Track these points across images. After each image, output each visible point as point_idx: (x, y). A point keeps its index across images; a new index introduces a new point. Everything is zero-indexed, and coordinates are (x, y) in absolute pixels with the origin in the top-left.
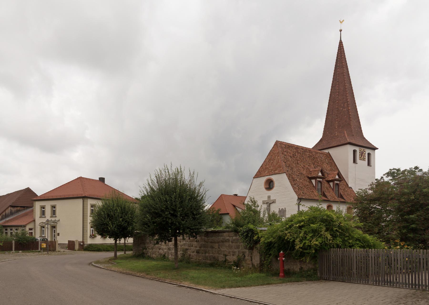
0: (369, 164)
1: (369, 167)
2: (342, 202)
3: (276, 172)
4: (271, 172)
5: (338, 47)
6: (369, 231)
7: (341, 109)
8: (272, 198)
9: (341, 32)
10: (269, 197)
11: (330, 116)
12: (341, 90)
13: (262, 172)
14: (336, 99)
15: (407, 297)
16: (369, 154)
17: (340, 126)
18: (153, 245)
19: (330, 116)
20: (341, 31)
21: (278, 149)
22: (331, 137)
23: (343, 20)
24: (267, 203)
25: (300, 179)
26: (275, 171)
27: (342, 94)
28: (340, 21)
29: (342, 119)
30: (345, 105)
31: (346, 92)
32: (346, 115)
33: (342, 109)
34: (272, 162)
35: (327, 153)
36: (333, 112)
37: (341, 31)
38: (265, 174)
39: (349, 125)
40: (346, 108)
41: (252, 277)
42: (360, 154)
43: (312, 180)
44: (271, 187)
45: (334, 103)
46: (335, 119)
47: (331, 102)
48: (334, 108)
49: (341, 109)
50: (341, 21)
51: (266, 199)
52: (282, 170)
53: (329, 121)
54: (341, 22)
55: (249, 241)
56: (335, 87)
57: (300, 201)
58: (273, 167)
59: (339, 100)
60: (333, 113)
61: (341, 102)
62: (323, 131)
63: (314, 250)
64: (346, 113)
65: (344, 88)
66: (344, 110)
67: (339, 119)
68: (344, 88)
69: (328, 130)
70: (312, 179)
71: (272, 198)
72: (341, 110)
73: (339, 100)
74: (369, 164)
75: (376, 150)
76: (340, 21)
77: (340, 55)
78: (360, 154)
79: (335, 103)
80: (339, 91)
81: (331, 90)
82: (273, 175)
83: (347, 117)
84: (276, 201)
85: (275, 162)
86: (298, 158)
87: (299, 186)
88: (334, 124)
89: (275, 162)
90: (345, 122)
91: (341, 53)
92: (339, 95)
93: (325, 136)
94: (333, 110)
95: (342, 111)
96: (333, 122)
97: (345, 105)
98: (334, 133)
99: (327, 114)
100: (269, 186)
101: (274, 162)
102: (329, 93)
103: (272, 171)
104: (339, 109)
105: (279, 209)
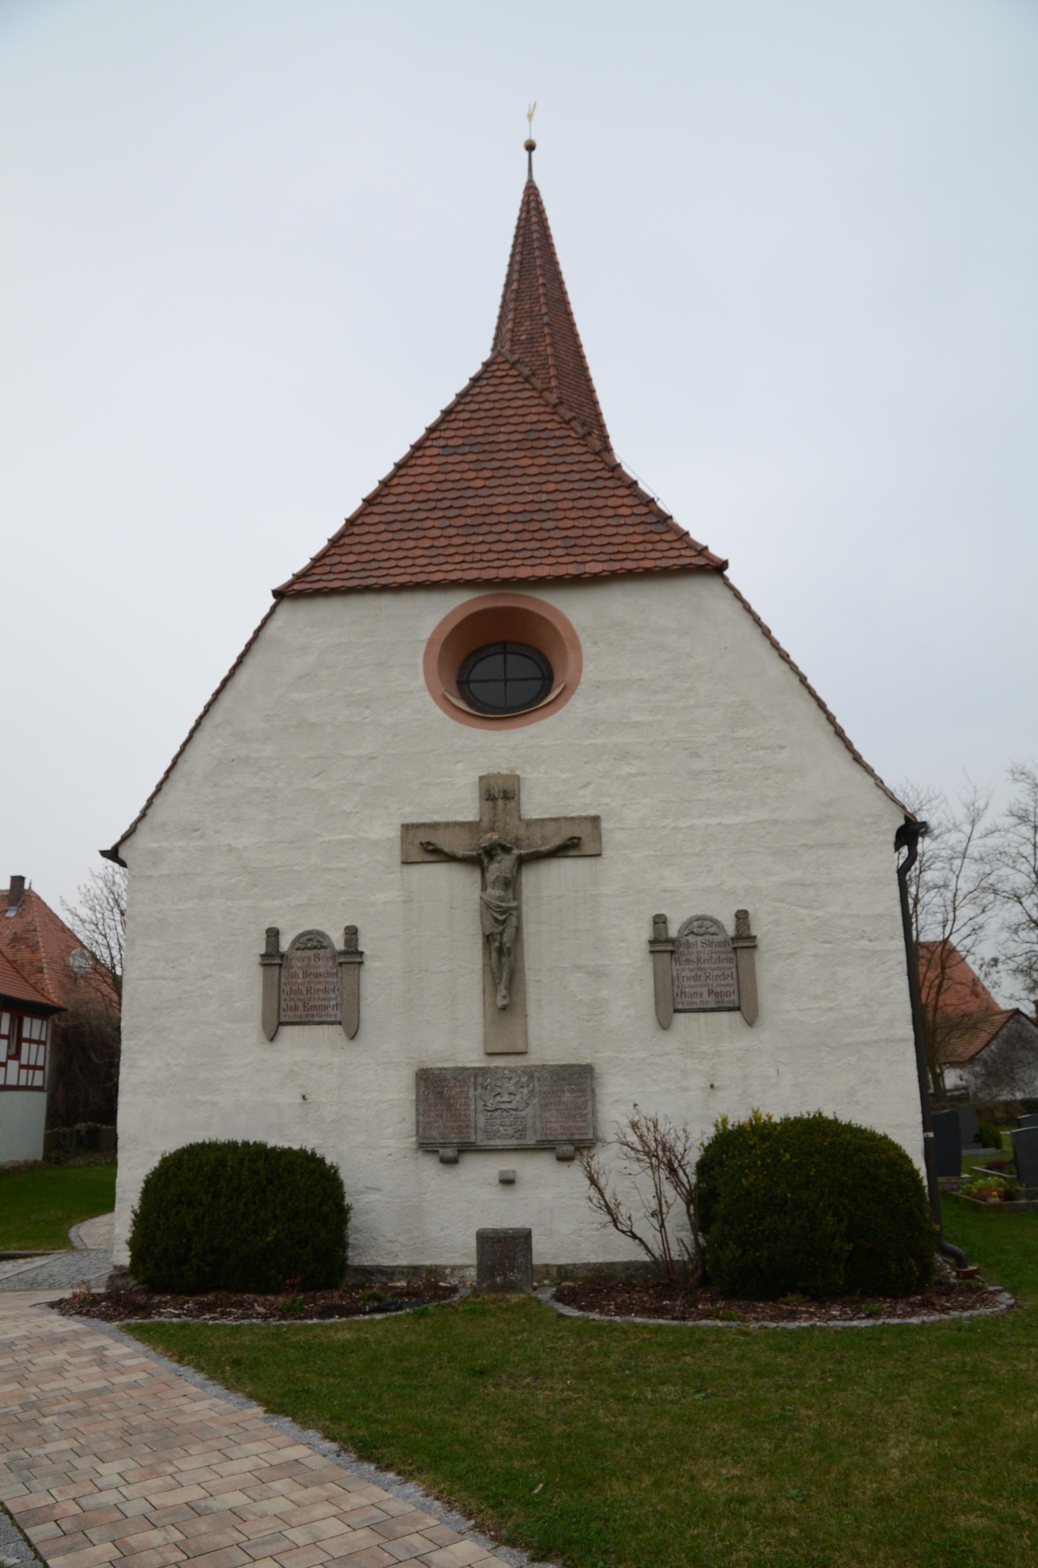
9: (534, 153)
20: (530, 147)
37: (530, 147)
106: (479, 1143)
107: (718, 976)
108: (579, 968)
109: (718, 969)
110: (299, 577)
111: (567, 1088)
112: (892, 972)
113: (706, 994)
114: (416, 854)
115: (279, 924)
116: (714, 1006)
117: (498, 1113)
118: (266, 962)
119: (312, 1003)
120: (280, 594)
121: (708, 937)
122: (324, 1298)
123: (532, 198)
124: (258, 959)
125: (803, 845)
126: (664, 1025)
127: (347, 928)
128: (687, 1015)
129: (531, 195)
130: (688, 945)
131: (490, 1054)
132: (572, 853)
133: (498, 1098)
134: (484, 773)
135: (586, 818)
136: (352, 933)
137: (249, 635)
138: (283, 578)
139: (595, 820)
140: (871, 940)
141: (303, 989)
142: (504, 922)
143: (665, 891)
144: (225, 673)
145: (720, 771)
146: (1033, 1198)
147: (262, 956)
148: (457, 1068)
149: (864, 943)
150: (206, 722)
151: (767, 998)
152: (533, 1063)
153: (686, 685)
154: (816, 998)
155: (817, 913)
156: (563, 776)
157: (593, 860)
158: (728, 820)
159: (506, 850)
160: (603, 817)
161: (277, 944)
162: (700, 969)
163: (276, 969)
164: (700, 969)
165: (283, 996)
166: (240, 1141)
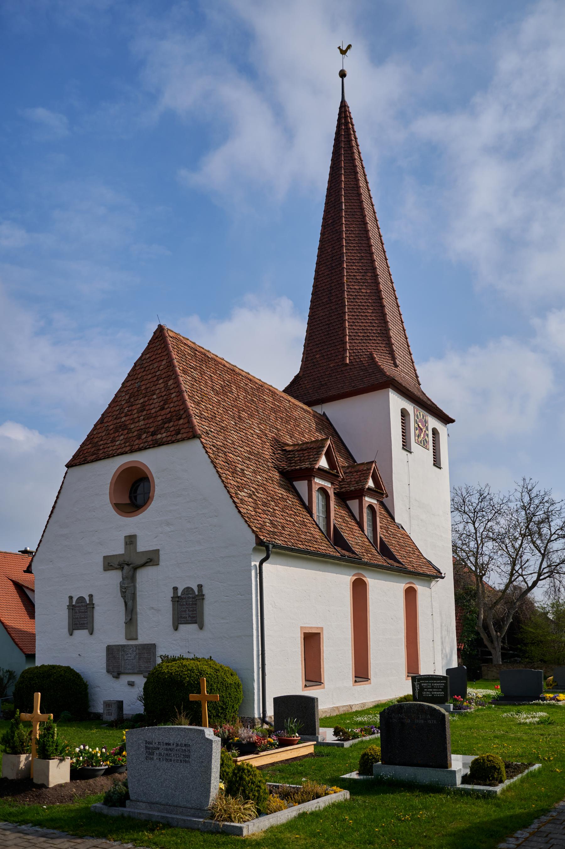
1: (162, 557)
2: (342, 559)
3: (159, 436)
4: (139, 438)
5: (339, 106)
8: (142, 546)
9: (345, 79)
10: (131, 540)
11: (323, 307)
13: (102, 442)
19: (323, 307)
20: (343, 74)
21: (165, 353)
22: (329, 369)
23: (349, 47)
24: (121, 567)
25: (254, 472)
26: (154, 434)
28: (339, 48)
34: (142, 401)
35: (320, 414)
37: (343, 74)
38: (115, 448)
43: (294, 483)
44: (140, 500)
48: (333, 285)
50: (344, 49)
51: (118, 549)
52: (185, 426)
54: (343, 52)
56: (335, 226)
57: (264, 556)
58: (146, 422)
60: (331, 298)
62: (303, 354)
69: (318, 349)
70: (296, 481)
71: (142, 546)
76: (341, 48)
79: (336, 270)
81: (322, 234)
82: (145, 449)
84: (161, 558)
85: (155, 401)
86: (241, 403)
87: (257, 497)
88: (337, 330)
89: (155, 401)
93: (309, 366)
96: (334, 324)
98: (340, 357)
100: (130, 498)
101: (149, 400)
103: (144, 436)
105: (175, 589)
106: (122, 671)
107: (192, 610)
110: (71, 460)
113: (188, 617)
117: (127, 661)
119: (81, 622)
120: (69, 466)
122: (426, 808)
123: (343, 110)
124: (171, 599)
126: (176, 629)
129: (344, 108)
132: (151, 564)
133: (127, 656)
136: (91, 596)
138: (68, 458)
139: (158, 551)
141: (79, 617)
142: (125, 592)
145: (197, 528)
147: (172, 597)
152: (141, 643)
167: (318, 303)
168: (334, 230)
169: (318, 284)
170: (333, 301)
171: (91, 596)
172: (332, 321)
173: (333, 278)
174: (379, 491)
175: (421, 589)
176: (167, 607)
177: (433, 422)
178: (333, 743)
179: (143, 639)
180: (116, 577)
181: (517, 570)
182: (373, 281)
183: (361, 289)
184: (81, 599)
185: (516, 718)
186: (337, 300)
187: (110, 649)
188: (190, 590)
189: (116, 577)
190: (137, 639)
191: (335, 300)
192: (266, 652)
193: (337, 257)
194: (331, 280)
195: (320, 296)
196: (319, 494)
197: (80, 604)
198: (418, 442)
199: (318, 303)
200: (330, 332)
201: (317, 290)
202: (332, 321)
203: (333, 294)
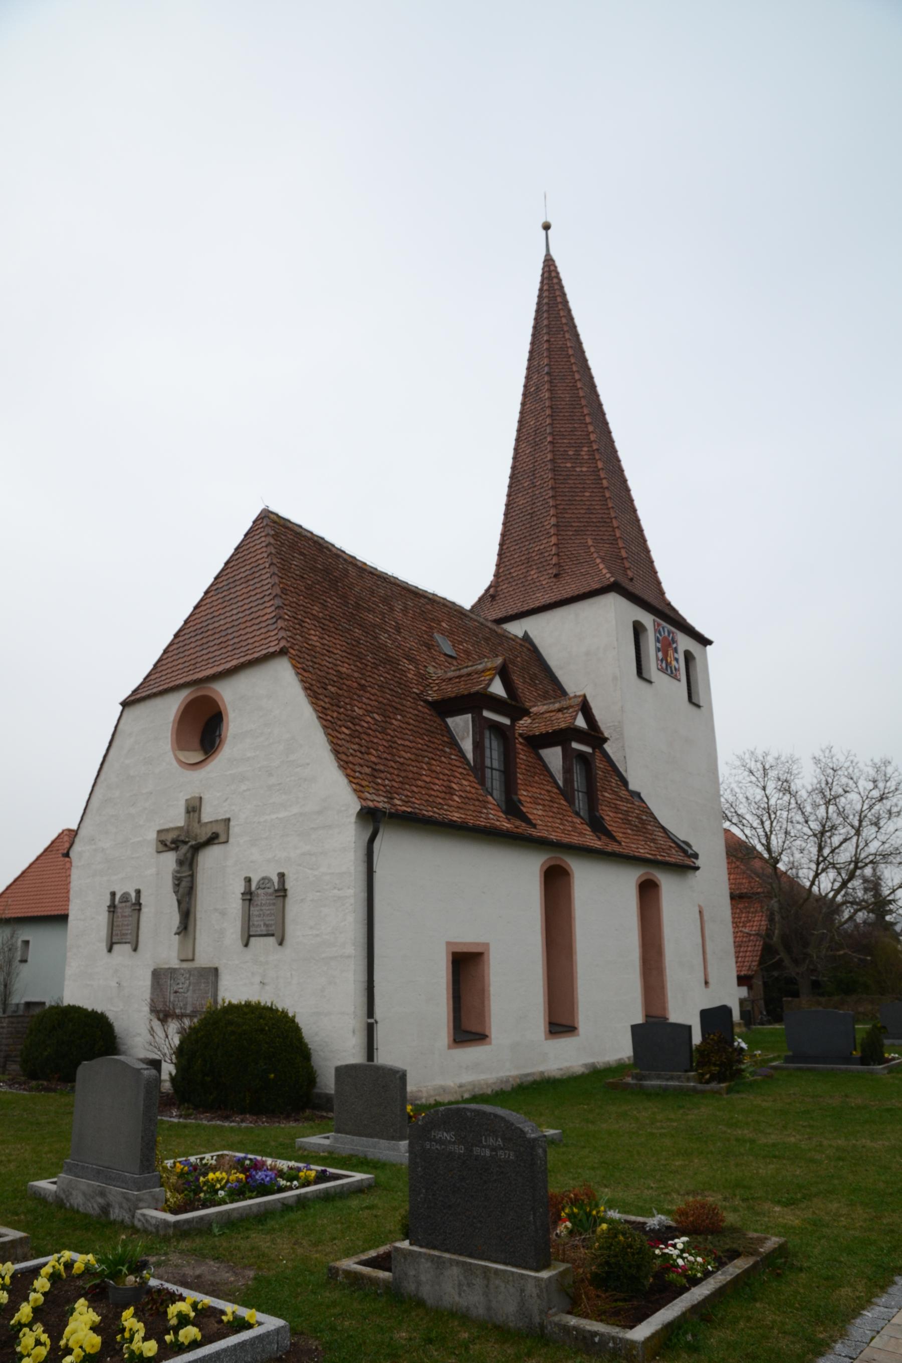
0: (692, 698)
1: (235, 829)
6: (217, 1258)
7: (569, 465)
9: (550, 232)
10: (193, 808)
12: (563, 403)
14: (545, 430)
15: (384, 690)
16: (689, 657)
17: (566, 526)
18: (858, 891)
20: (547, 227)
27: (566, 414)
29: (574, 502)
30: (583, 453)
31: (580, 410)
32: (590, 490)
33: (572, 467)
36: (536, 478)
37: (547, 227)
39: (603, 526)
40: (585, 465)
41: (76, 1265)
42: (659, 645)
45: (538, 445)
46: (544, 499)
47: (523, 446)
48: (536, 464)
49: (566, 467)
53: (518, 512)
55: (851, 891)
59: (557, 435)
60: (535, 481)
61: (565, 441)
63: (785, 873)
64: (588, 482)
65: (571, 397)
66: (578, 469)
67: (563, 503)
68: (571, 397)
71: (208, 814)
72: (569, 471)
73: (557, 435)
74: (692, 698)
75: (708, 647)
77: (551, 295)
78: (659, 645)
80: (554, 403)
81: (523, 404)
83: (593, 494)
88: (543, 520)
90: (586, 513)
91: (550, 278)
92: (557, 418)
94: (534, 471)
95: (574, 473)
97: (583, 453)
99: (510, 487)
102: (516, 416)
104: (559, 467)
108: (216, 910)
109: (268, 910)
111: (203, 981)
112: (347, 911)
114: (161, 848)
115: (251, 875)
116: (265, 933)
118: (245, 898)
120: (126, 704)
121: (266, 890)
124: (107, 908)
125: (312, 828)
127: (246, 878)
128: (699, 921)
130: (258, 895)
131: (182, 961)
132: (216, 841)
134: (189, 797)
135: (222, 820)
136: (138, 892)
137: (112, 729)
140: (339, 890)
143: (252, 862)
144: (104, 752)
146: (641, 1080)
148: (169, 968)
149: (336, 891)
150: (99, 781)
151: (291, 930)
152: (198, 966)
153: (269, 730)
154: (311, 928)
155: (316, 873)
156: (218, 795)
157: (225, 845)
158: (282, 815)
159: (185, 843)
160: (231, 819)
161: (250, 886)
162: (261, 910)
163: (281, 898)
164: (261, 910)
165: (114, 928)
166: (280, 1010)
167: (517, 488)
168: (538, 398)
169: (517, 464)
170: (537, 484)
171: (138, 892)
172: (536, 510)
173: (537, 456)
174: (593, 733)
175: (668, 885)
176: (235, 905)
177: (684, 642)
178: (352, 1171)
179: (203, 959)
180: (170, 860)
181: (825, 855)
182: (591, 457)
183: (575, 467)
184: (125, 897)
185: (180, 1259)
186: (543, 482)
187: (157, 975)
188: (267, 881)
189: (170, 860)
190: (193, 960)
191: (539, 483)
192: (376, 984)
193: (542, 430)
194: (534, 458)
195: (520, 478)
196: (493, 737)
197: (124, 904)
198: (662, 668)
199: (517, 488)
200: (533, 524)
201: (516, 472)
202: (536, 510)
203: (538, 475)
